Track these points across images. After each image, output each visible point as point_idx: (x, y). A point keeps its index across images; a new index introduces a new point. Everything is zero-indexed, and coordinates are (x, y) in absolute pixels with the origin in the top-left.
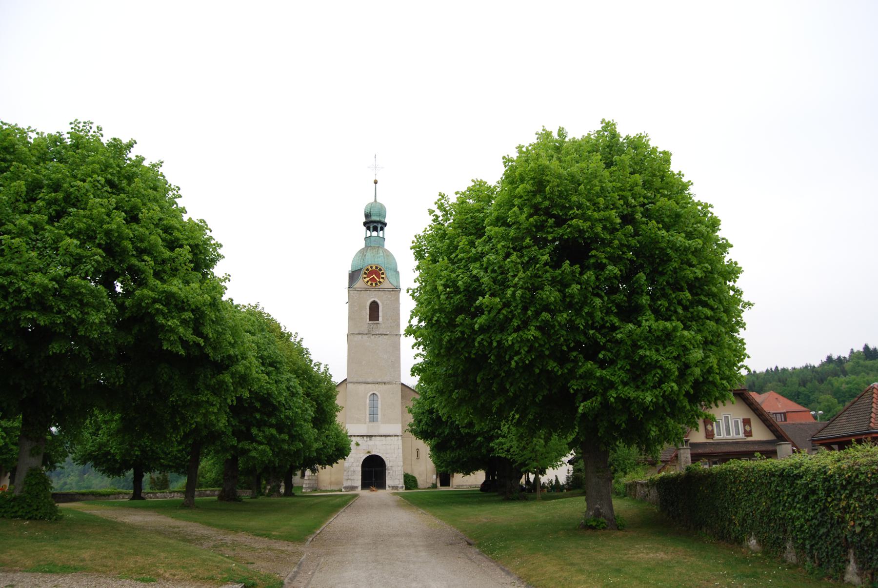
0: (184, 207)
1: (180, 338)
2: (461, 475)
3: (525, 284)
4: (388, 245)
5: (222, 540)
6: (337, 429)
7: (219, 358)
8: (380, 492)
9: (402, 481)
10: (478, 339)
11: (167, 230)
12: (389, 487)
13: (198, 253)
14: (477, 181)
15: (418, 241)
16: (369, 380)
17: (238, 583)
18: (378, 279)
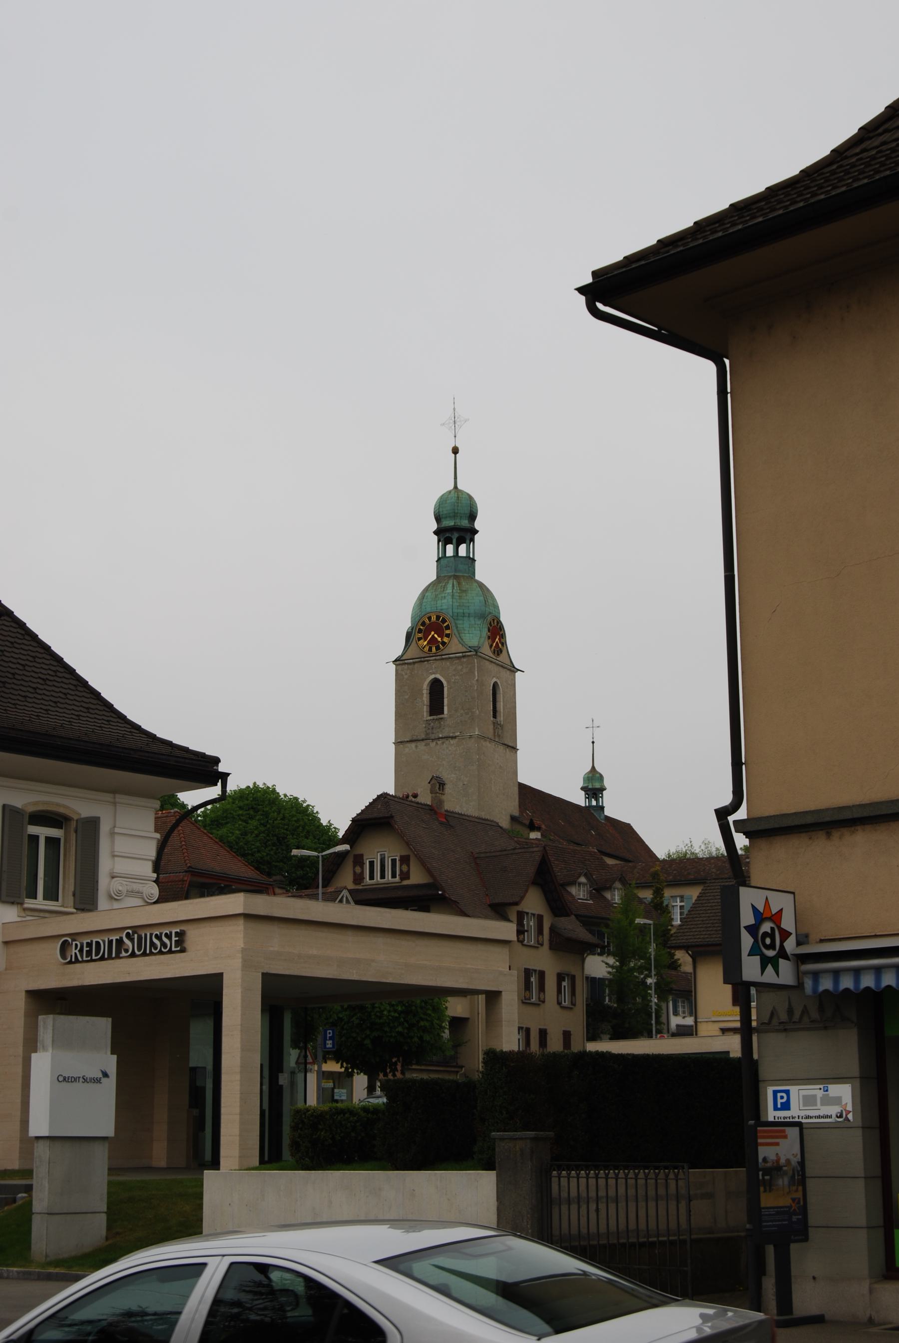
18: (439, 639)
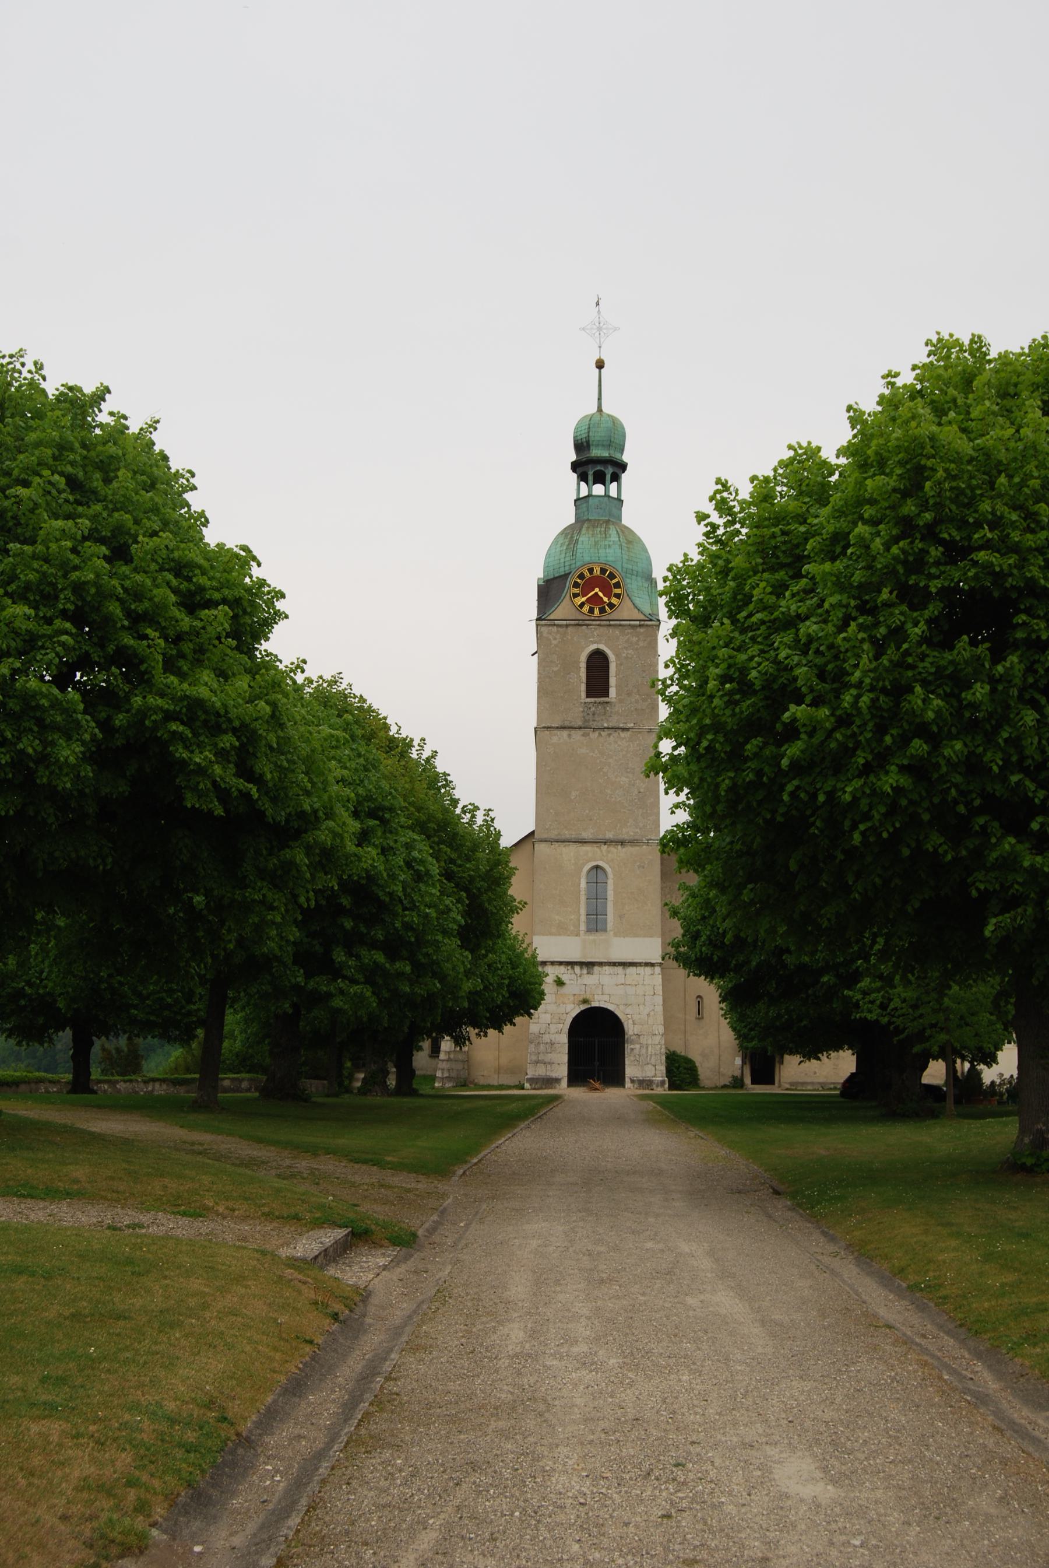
0: (203, 511)
1: (214, 783)
2: (797, 1058)
3: (878, 682)
4: (628, 517)
5: (289, 1167)
6: (512, 948)
7: (282, 817)
8: (612, 1095)
9: (662, 1068)
10: (790, 788)
11: (181, 569)
12: (632, 1081)
13: (241, 613)
14: (801, 447)
15: (675, 577)
16: (586, 835)
17: (340, 1227)
18: (606, 599)
